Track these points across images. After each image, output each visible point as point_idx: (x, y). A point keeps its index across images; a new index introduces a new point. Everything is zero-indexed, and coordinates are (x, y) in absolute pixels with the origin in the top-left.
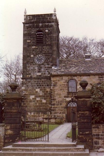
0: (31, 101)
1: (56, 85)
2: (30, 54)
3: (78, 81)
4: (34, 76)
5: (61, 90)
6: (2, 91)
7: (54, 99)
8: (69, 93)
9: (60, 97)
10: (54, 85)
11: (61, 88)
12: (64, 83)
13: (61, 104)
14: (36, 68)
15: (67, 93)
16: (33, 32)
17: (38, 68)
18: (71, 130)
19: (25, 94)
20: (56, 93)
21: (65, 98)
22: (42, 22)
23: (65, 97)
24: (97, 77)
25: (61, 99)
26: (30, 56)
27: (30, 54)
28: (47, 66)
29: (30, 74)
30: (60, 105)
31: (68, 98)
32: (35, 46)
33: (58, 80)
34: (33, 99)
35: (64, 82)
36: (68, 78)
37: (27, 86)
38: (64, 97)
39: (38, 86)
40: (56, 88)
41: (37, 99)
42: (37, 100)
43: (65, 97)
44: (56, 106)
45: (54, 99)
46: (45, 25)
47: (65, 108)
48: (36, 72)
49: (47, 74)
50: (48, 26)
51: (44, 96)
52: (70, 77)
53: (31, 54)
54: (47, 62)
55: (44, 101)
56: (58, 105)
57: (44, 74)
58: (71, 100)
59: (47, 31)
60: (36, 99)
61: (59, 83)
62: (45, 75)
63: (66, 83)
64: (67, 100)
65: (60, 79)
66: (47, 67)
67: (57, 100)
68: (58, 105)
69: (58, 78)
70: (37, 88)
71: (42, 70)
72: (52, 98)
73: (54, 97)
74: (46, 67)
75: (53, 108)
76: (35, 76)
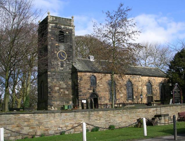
0: (56, 92)
7: (80, 91)
9: (85, 90)
12: (87, 78)
13: (86, 95)
14: (60, 63)
17: (61, 63)
18: (150, 16)
19: (51, 86)
20: (82, 86)
22: (64, 25)
23: (88, 89)
25: (85, 91)
28: (68, 62)
29: (54, 68)
34: (58, 90)
37: (53, 78)
38: (88, 90)
39: (61, 79)
40: (82, 82)
41: (62, 90)
43: (88, 89)
45: (80, 91)
51: (67, 88)
54: (68, 59)
55: (67, 92)
59: (67, 33)
60: (60, 90)
66: (69, 64)
67: (83, 91)
69: (83, 74)
70: (61, 81)
71: (65, 65)
74: (67, 64)
75: (80, 98)
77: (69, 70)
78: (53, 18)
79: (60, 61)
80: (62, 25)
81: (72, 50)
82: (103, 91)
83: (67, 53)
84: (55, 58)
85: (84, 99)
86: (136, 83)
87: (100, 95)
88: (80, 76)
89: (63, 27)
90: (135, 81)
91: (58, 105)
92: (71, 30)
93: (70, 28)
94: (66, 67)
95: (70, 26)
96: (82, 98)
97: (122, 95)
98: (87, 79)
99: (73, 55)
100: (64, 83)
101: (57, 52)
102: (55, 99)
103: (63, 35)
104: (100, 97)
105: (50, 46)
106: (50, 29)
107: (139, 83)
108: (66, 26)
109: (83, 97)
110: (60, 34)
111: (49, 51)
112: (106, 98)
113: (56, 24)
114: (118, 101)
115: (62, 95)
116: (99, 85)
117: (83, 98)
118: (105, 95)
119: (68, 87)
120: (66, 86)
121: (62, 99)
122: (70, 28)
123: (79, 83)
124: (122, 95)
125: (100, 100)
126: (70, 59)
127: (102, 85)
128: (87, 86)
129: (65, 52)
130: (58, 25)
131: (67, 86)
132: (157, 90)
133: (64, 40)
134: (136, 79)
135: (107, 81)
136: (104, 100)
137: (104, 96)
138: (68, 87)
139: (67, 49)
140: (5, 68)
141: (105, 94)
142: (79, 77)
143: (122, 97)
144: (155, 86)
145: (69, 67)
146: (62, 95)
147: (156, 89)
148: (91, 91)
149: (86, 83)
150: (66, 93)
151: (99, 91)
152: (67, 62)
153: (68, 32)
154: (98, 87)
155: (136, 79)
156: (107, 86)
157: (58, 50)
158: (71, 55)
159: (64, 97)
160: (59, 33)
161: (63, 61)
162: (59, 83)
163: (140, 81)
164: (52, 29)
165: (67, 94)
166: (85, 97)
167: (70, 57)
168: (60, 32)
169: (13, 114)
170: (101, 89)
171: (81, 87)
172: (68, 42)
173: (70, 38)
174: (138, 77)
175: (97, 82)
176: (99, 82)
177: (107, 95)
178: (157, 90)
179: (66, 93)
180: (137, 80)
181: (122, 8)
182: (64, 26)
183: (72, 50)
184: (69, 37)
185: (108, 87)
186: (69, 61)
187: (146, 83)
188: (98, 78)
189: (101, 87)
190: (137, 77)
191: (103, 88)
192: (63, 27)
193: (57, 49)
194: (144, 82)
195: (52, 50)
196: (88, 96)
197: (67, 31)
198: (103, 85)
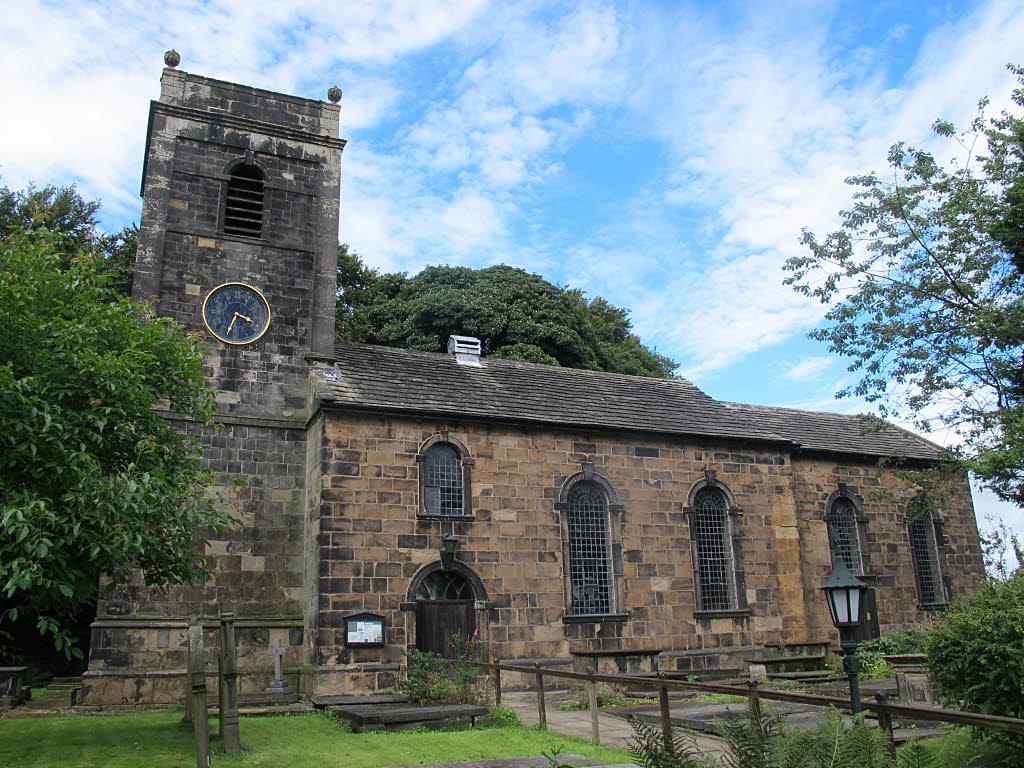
1: (355, 470)
3: (478, 456)
5: (385, 500)
9: (375, 542)
11: (385, 490)
12: (399, 463)
13: (381, 584)
15: (416, 522)
16: (211, 166)
17: (224, 364)
23: (404, 541)
24: (566, 447)
25: (380, 555)
27: (180, 275)
28: (277, 359)
31: (422, 547)
32: (214, 241)
35: (402, 456)
39: (215, 467)
40: (352, 485)
42: (207, 554)
43: (404, 541)
46: (281, 147)
47: (404, 608)
49: (273, 405)
50: (296, 159)
54: (280, 339)
56: (366, 588)
57: (260, 402)
58: (438, 562)
59: (288, 176)
62: (262, 409)
67: (361, 556)
68: (366, 588)
69: (365, 431)
71: (251, 377)
72: (331, 547)
73: (337, 540)
75: (336, 605)
79: (222, 347)
83: (273, 300)
85: (367, 617)
88: (339, 445)
89: (257, 139)
90: (750, 488)
91: (169, 654)
93: (310, 149)
95: (310, 139)
96: (345, 605)
97: (661, 584)
99: (321, 313)
102: (151, 610)
103: (259, 187)
104: (492, 597)
106: (166, 145)
107: (775, 497)
108: (281, 134)
109: (362, 597)
110: (232, 183)
111: (145, 283)
112: (543, 603)
113: (216, 119)
116: (486, 513)
117: (356, 604)
118: (535, 583)
119: (264, 527)
122: (310, 149)
124: (661, 584)
125: (494, 617)
128: (396, 515)
129: (266, 289)
130: (227, 131)
131: (259, 517)
132: (893, 548)
133: (229, 203)
135: (550, 483)
137: (524, 588)
140: (50, 441)
141: (533, 573)
142: (336, 451)
143: (660, 595)
145: (281, 389)
148: (426, 557)
151: (490, 557)
153: (293, 170)
154: (479, 529)
155: (756, 471)
157: (210, 279)
159: (227, 595)
160: (229, 177)
161: (246, 347)
163: (780, 490)
164: (177, 149)
165: (250, 575)
166: (373, 598)
167: (293, 323)
168: (241, 169)
170: (504, 539)
171: (349, 527)
175: (477, 490)
176: (486, 492)
177: (553, 581)
178: (893, 548)
180: (765, 479)
181: (918, 391)
182: (264, 138)
188: (479, 463)
189: (502, 528)
191: (517, 530)
192: (257, 139)
193: (205, 271)
195: (170, 277)
196: (401, 587)
197: (284, 167)
198: (524, 514)
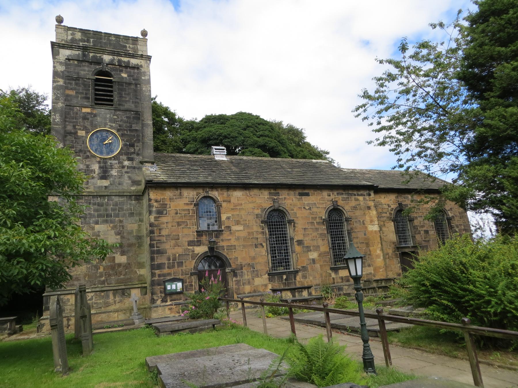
1: (165, 212)
2: (74, 127)
3: (224, 201)
4: (87, 188)
5: (180, 225)
6: (3, 96)
8: (200, 233)
9: (177, 245)
10: (160, 213)
11: (180, 220)
12: (186, 207)
13: (180, 264)
14: (96, 167)
16: (85, 73)
17: (100, 167)
20: (164, 232)
21: (191, 248)
22: (112, 53)
23: (191, 243)
25: (179, 250)
26: (77, 132)
28: (126, 163)
30: (178, 266)
31: (199, 245)
32: (90, 109)
33: (170, 199)
35: (187, 204)
36: (195, 193)
39: (99, 216)
40: (164, 219)
43: (191, 243)
44: (166, 271)
46: (119, 61)
47: (192, 274)
48: (93, 178)
50: (127, 66)
52: (201, 191)
53: (77, 127)
54: (127, 154)
57: (119, 184)
58: (207, 252)
59: (124, 75)
61: (172, 204)
63: (191, 207)
64: (196, 252)
65: (175, 196)
67: (170, 252)
69: (169, 194)
71: (114, 172)
72: (155, 249)
75: (159, 276)
76: (91, 189)
77: (132, 186)
78: (72, 34)
79: (98, 159)
80: (104, 52)
81: (143, 124)
82: (244, 246)
84: (80, 151)
85: (175, 280)
86: (358, 213)
87: (237, 258)
88: (156, 201)
89: (107, 58)
90: (355, 208)
92: (138, 68)
93: (134, 61)
94: (120, 177)
95: (133, 56)
96: (164, 275)
97: (314, 255)
98: (184, 210)
100: (113, 228)
101: (87, 133)
104: (234, 266)
105: (61, 116)
109: (172, 271)
112: (258, 267)
113: (85, 49)
114: (300, 274)
115: (101, 270)
116: (229, 227)
117: (169, 274)
118: (254, 258)
119: (125, 242)
120: (118, 237)
121: (103, 282)
122: (134, 61)
123: (156, 223)
124: (314, 255)
126: (134, 153)
127: (241, 228)
128: (186, 231)
129: (118, 130)
131: (122, 237)
132: (427, 232)
134: (357, 203)
135: (259, 212)
136: (250, 277)
137: (248, 261)
138: (125, 242)
139: (125, 122)
142: (155, 204)
143: (314, 260)
144: (419, 219)
145: (130, 178)
146: (101, 270)
147: (425, 229)
149: (179, 224)
150: (117, 261)
151: (231, 248)
152: (122, 163)
156: (260, 230)
157: (89, 127)
158: (138, 141)
159: (110, 275)
161: (110, 159)
162: (93, 228)
164: (66, 65)
165: (119, 265)
166: (177, 271)
169: (292, 327)
170: (238, 239)
171: (164, 239)
172: (129, 101)
173: (135, 91)
174: (362, 195)
176: (228, 218)
178: (427, 232)
179: (117, 261)
180: (362, 203)
182: (111, 57)
183: (142, 128)
184: (133, 87)
185: (263, 233)
186: (130, 159)
187: (390, 214)
188: (224, 204)
190: (358, 195)
191: (244, 234)
192: (107, 58)
194: (384, 211)
195: (69, 128)
197: (121, 71)
198: (245, 225)
